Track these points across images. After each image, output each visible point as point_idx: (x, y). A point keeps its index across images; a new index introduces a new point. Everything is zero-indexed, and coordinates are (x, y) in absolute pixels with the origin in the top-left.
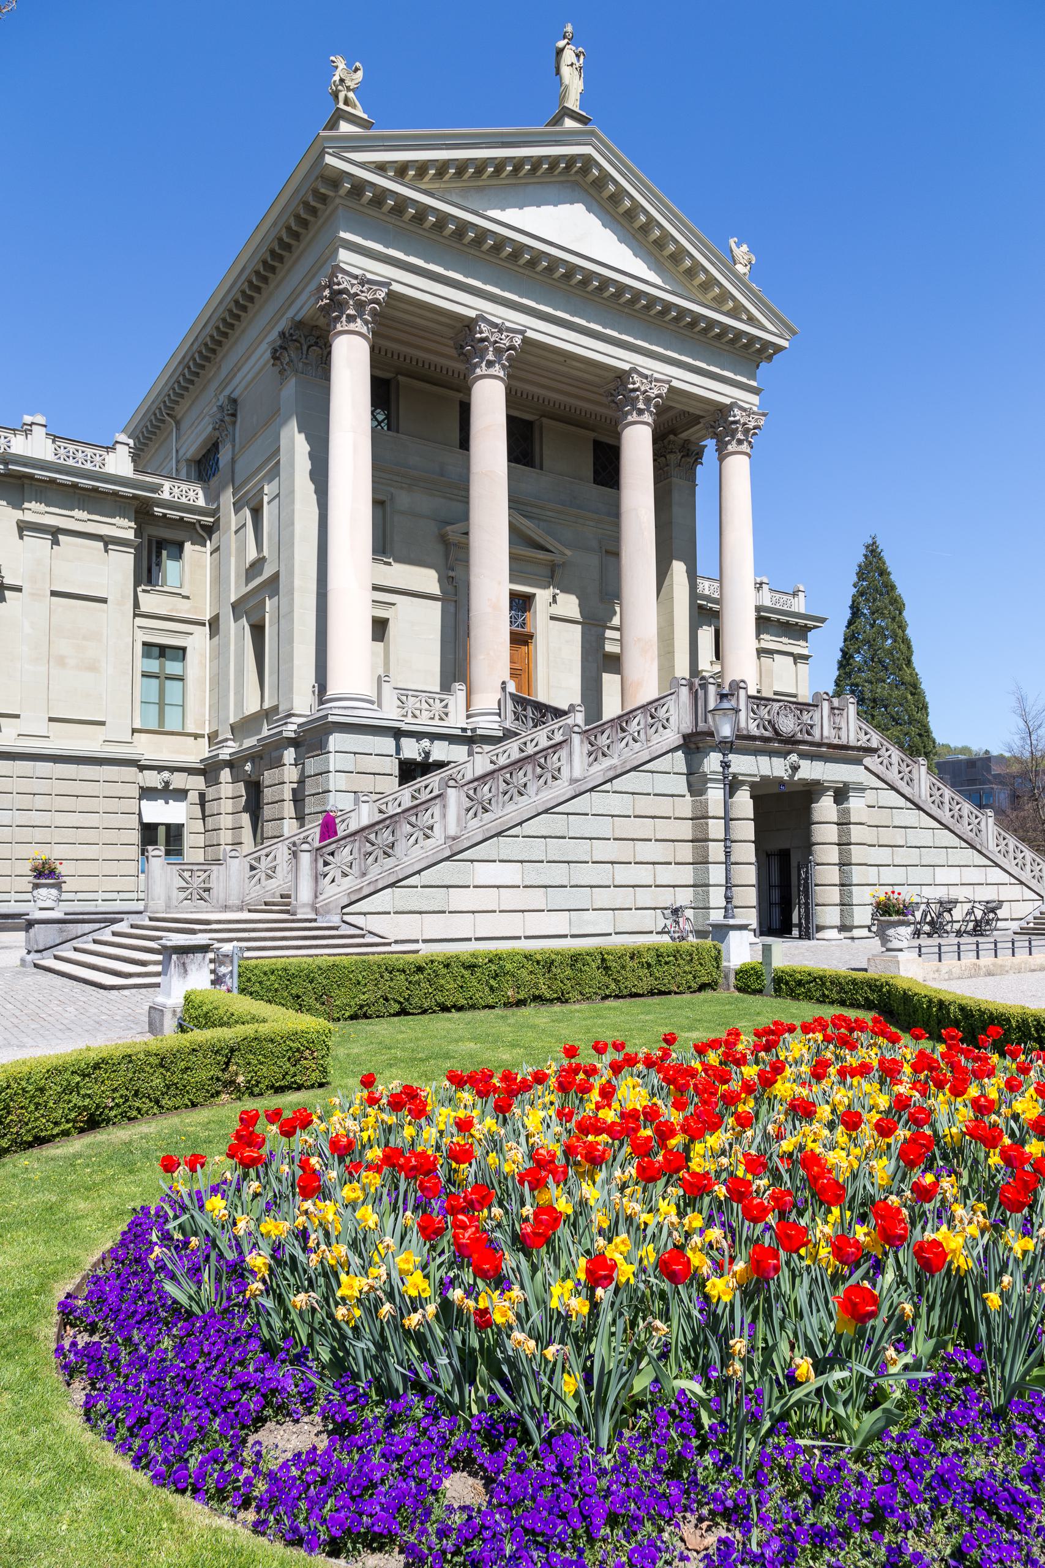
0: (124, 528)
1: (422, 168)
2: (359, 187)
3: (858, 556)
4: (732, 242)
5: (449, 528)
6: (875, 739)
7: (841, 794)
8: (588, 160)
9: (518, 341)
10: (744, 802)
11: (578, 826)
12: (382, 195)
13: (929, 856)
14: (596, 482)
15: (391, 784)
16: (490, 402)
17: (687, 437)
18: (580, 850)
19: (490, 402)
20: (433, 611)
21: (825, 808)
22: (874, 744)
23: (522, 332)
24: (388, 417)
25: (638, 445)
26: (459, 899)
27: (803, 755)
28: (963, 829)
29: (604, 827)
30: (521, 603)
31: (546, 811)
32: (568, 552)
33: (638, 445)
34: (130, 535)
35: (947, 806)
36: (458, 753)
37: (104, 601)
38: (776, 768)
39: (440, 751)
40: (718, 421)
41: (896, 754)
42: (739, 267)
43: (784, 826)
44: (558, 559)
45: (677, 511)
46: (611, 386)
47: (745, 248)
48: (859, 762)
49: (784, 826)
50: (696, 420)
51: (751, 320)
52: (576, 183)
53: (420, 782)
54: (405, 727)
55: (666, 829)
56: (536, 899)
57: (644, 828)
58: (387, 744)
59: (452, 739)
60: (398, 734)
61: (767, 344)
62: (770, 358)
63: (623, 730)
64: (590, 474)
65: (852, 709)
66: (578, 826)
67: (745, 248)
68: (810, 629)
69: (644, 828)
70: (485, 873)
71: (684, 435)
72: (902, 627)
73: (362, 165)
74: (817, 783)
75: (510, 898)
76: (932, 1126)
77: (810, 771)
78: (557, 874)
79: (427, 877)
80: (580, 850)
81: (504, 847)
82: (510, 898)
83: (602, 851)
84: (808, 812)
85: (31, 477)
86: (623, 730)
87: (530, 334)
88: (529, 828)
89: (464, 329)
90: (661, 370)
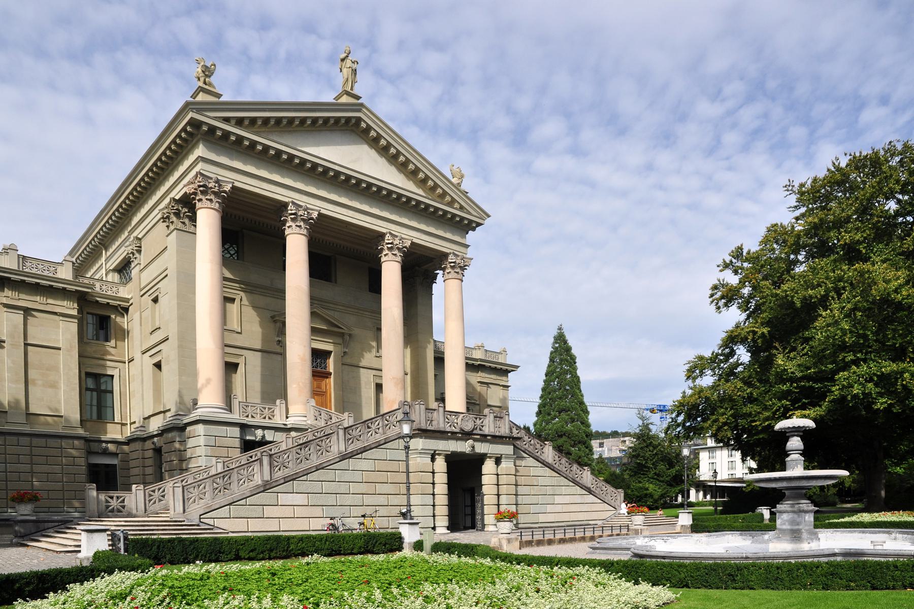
0: (70, 307)
1: (253, 121)
2: (212, 129)
3: (555, 332)
7: (498, 461)
8: (359, 120)
10: (441, 465)
12: (226, 134)
13: (549, 490)
15: (236, 453)
17: (421, 270)
18: (343, 488)
20: (8, 437)
21: (488, 467)
24: (237, 252)
25: (391, 273)
26: (268, 511)
27: (475, 440)
29: (357, 476)
30: (318, 356)
33: (391, 273)
34: (75, 312)
36: (279, 436)
37: (59, 349)
38: (464, 447)
39: (269, 436)
43: (464, 476)
49: (464, 476)
52: (352, 131)
53: (252, 453)
55: (391, 477)
57: (381, 477)
59: (277, 429)
60: (244, 427)
61: (471, 221)
63: (369, 427)
64: (367, 286)
68: (510, 372)
69: (381, 477)
70: (283, 499)
72: (575, 369)
73: (215, 118)
75: (299, 511)
77: (481, 448)
78: (331, 500)
80: (343, 488)
82: (299, 511)
85: (9, 279)
86: (369, 427)
90: (401, 232)
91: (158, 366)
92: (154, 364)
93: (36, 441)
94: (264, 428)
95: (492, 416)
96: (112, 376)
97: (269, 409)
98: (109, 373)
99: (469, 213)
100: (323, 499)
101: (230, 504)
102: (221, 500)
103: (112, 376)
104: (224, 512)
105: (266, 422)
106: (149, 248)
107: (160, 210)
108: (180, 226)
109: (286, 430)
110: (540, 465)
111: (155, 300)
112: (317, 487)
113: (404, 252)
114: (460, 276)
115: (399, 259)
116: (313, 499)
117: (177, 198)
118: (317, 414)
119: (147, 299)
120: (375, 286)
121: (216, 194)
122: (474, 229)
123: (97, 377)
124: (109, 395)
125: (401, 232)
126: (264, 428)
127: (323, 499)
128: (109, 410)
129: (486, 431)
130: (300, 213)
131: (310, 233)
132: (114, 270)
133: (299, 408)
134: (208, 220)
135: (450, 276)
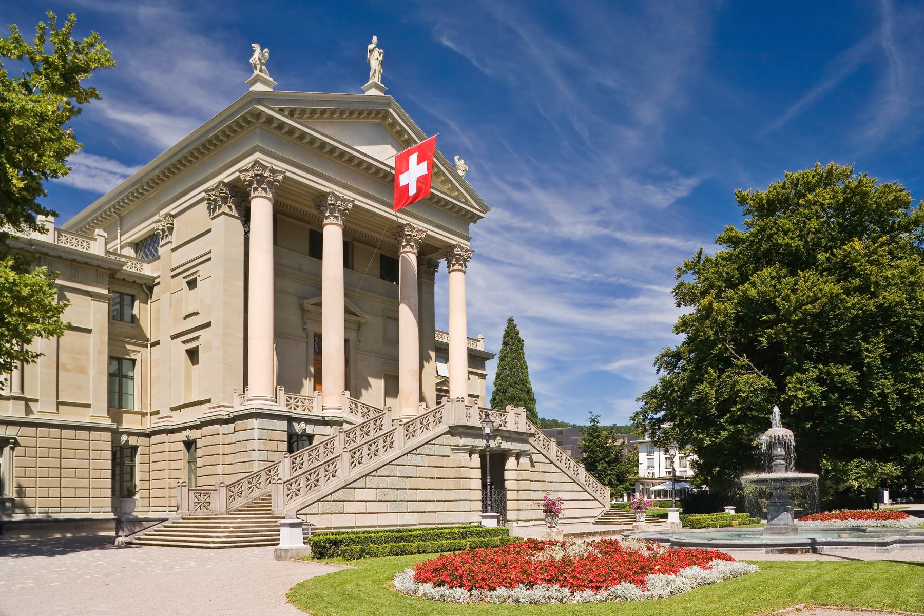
4: (456, 158)
5: (305, 301)
6: (533, 429)
9: (350, 206)
11: (400, 471)
14: (382, 277)
16: (333, 238)
17: (431, 256)
19: (333, 238)
21: (511, 463)
22: (532, 431)
23: (352, 202)
28: (571, 473)
31: (388, 464)
32: (367, 317)
35: (572, 469)
37: (89, 331)
39: (310, 429)
40: (448, 252)
41: (542, 437)
42: (459, 172)
44: (363, 321)
45: (424, 296)
46: (395, 231)
47: (462, 162)
48: (527, 442)
49: (493, 467)
50: (437, 249)
51: (466, 202)
54: (293, 415)
56: (383, 507)
58: (284, 425)
60: (290, 420)
62: (475, 222)
65: (524, 415)
66: (400, 471)
67: (462, 162)
70: (359, 494)
71: (429, 256)
74: (509, 450)
76: (659, 571)
77: (506, 445)
79: (333, 497)
81: (369, 481)
83: (166, 456)
84: (504, 465)
87: (356, 202)
88: (379, 473)
89: (320, 198)
90: (421, 227)
91: (193, 355)
92: (187, 351)
93: (65, 433)
94: (308, 421)
95: (513, 412)
96: (134, 361)
97: (295, 399)
98: (133, 357)
99: (466, 202)
100: (391, 495)
101: (319, 500)
102: (314, 495)
103: (134, 361)
104: (314, 508)
105: (306, 414)
106: (184, 227)
107: (206, 191)
108: (227, 210)
109: (324, 422)
110: (547, 461)
111: (192, 284)
112: (390, 482)
113: (420, 244)
114: (464, 269)
115: (415, 251)
116: (380, 494)
117: (226, 181)
118: (353, 406)
119: (181, 282)
120: (316, 249)
121: (270, 184)
122: (475, 222)
123: (119, 360)
124: (130, 382)
125: (421, 227)
126: (308, 421)
127: (391, 495)
128: (130, 397)
129: (510, 427)
130: (339, 203)
131: (344, 223)
132: (130, 244)
133: (331, 398)
134: (262, 209)
135: (455, 268)
